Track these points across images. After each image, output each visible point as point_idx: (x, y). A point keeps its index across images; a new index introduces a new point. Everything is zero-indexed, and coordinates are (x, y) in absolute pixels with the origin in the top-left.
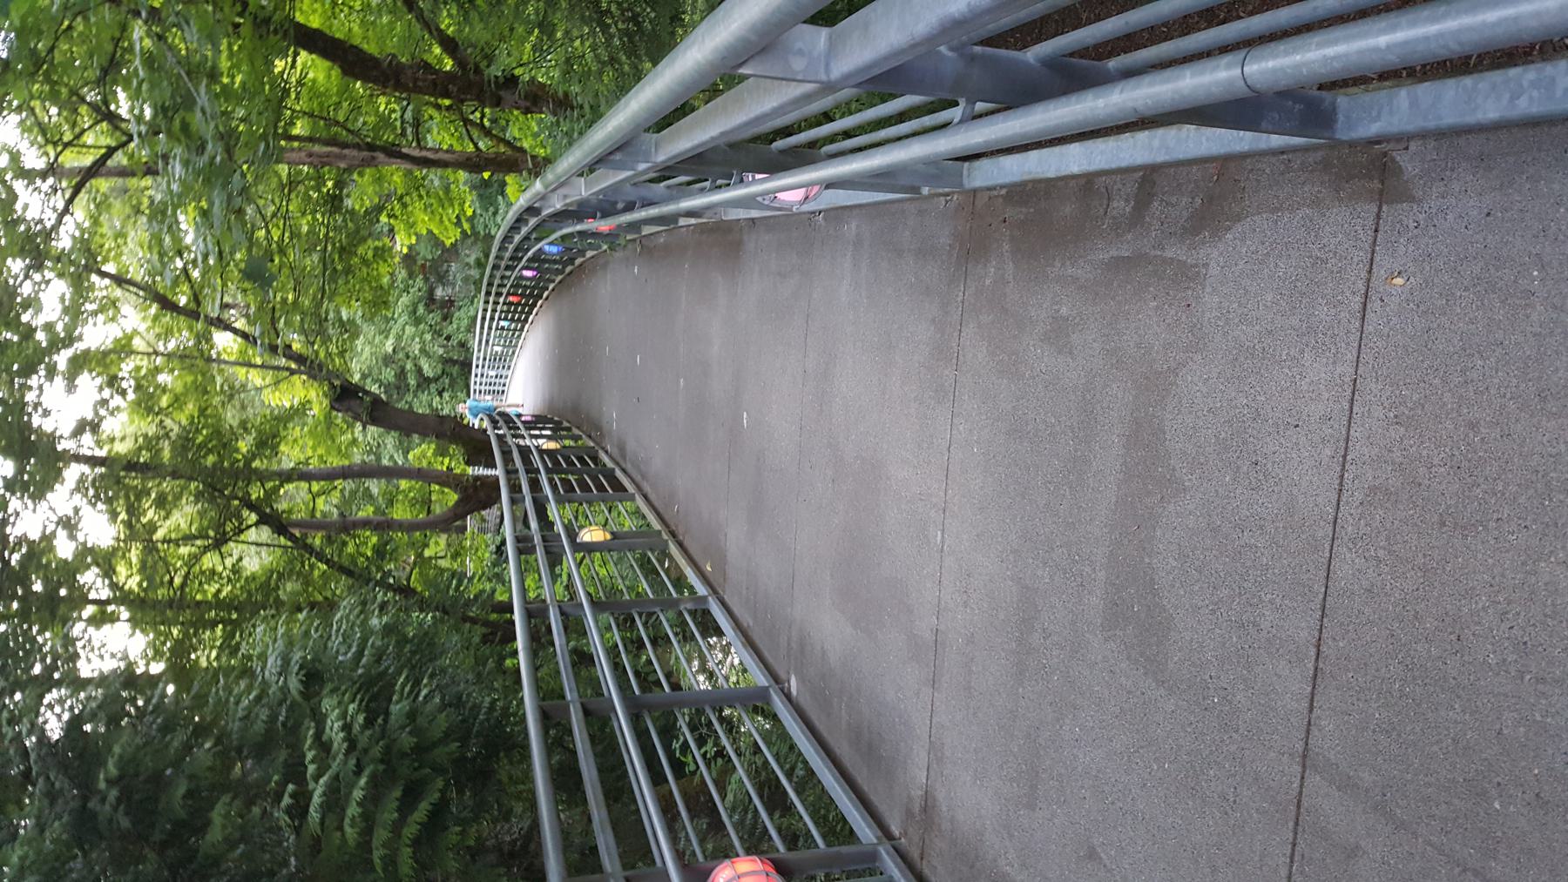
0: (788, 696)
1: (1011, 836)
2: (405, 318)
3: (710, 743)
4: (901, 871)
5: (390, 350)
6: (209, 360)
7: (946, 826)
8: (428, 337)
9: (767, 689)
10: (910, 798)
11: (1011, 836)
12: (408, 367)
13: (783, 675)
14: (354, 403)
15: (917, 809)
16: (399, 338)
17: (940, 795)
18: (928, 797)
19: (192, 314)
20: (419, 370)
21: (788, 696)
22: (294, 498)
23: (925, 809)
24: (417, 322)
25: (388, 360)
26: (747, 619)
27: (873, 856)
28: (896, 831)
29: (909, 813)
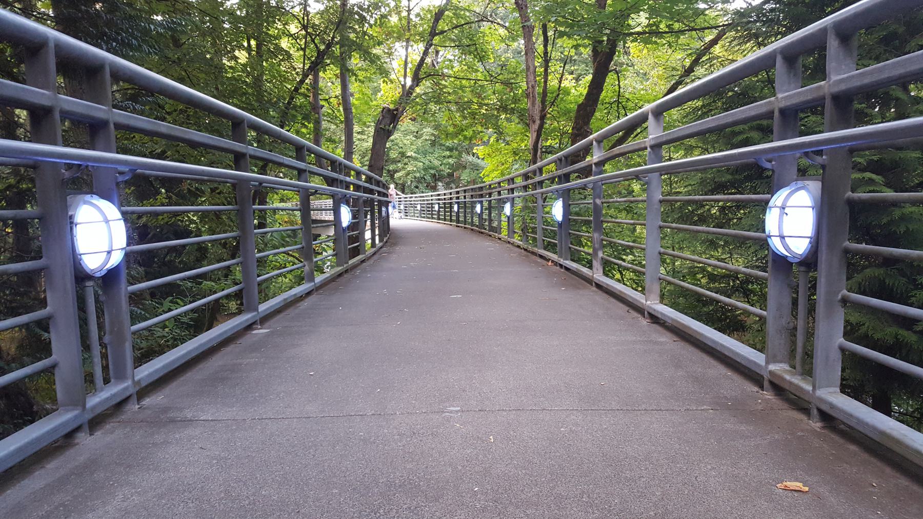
0: (249, 327)
1: (161, 497)
2: (427, 163)
3: (167, 323)
4: (107, 399)
5: (409, 154)
6: (408, 40)
7: (159, 438)
8: (418, 175)
9: (257, 310)
10: (181, 410)
11: (161, 497)
12: (399, 165)
13: (267, 324)
14: (387, 121)
15: (171, 415)
16: (416, 159)
17: (189, 431)
18: (188, 422)
19: (433, 34)
20: (396, 171)
21: (249, 327)
22: (329, 80)
23: (173, 421)
24: (425, 169)
25: (403, 154)
26: (305, 304)
27: (121, 377)
28: (147, 402)
29: (166, 410)
